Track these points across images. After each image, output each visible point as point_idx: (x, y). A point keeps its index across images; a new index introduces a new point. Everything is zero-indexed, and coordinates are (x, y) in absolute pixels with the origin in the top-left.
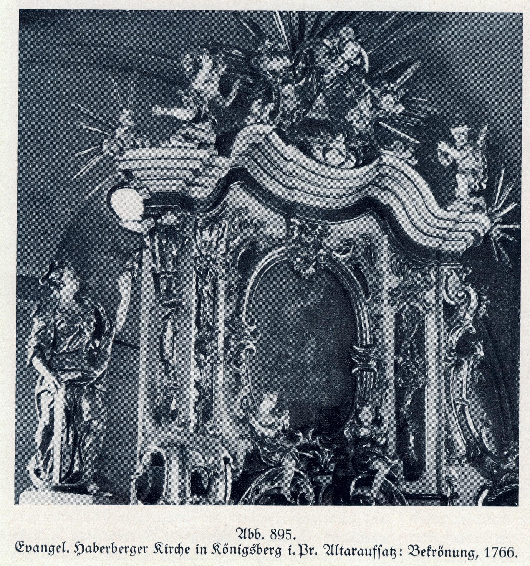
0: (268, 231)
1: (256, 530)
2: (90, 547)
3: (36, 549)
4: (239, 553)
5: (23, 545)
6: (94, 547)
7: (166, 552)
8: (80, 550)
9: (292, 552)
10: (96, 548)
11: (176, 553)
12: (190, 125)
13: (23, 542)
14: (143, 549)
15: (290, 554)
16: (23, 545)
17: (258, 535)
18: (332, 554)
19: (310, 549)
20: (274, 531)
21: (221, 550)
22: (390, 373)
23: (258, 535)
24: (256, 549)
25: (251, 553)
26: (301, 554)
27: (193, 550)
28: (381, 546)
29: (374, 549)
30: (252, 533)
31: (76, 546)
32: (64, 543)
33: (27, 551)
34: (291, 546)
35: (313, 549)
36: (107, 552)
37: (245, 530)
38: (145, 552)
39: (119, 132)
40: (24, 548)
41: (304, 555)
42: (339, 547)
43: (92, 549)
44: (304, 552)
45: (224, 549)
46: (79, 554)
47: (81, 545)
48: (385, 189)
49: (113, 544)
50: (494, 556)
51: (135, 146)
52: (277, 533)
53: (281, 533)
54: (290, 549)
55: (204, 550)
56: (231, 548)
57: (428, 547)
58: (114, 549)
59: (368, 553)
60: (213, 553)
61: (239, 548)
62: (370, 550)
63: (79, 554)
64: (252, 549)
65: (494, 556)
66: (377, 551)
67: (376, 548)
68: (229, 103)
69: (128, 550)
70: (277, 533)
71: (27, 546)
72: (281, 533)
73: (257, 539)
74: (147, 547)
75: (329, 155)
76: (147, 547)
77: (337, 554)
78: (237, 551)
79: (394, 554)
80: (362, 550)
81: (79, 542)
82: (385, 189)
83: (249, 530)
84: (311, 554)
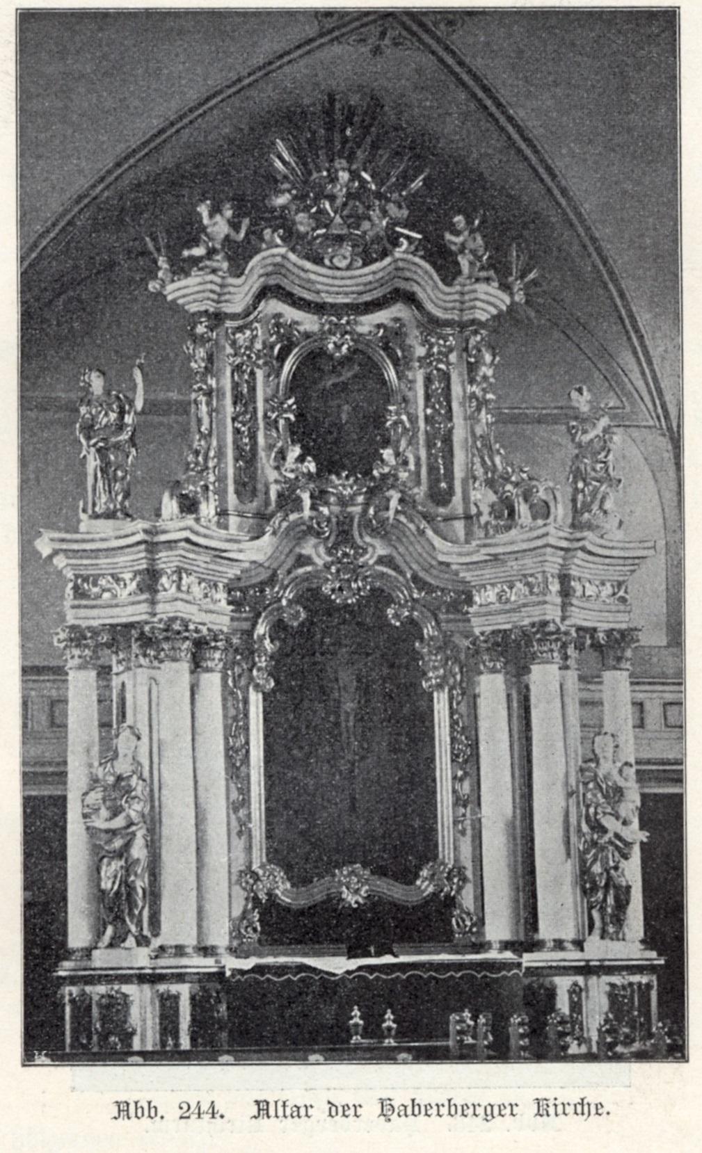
0: (301, 328)
6: (413, 1106)
12: (209, 259)
22: (422, 424)
39: (160, 274)
43: (409, 1111)
51: (173, 281)
58: (453, 1109)
68: (242, 235)
75: (335, 260)
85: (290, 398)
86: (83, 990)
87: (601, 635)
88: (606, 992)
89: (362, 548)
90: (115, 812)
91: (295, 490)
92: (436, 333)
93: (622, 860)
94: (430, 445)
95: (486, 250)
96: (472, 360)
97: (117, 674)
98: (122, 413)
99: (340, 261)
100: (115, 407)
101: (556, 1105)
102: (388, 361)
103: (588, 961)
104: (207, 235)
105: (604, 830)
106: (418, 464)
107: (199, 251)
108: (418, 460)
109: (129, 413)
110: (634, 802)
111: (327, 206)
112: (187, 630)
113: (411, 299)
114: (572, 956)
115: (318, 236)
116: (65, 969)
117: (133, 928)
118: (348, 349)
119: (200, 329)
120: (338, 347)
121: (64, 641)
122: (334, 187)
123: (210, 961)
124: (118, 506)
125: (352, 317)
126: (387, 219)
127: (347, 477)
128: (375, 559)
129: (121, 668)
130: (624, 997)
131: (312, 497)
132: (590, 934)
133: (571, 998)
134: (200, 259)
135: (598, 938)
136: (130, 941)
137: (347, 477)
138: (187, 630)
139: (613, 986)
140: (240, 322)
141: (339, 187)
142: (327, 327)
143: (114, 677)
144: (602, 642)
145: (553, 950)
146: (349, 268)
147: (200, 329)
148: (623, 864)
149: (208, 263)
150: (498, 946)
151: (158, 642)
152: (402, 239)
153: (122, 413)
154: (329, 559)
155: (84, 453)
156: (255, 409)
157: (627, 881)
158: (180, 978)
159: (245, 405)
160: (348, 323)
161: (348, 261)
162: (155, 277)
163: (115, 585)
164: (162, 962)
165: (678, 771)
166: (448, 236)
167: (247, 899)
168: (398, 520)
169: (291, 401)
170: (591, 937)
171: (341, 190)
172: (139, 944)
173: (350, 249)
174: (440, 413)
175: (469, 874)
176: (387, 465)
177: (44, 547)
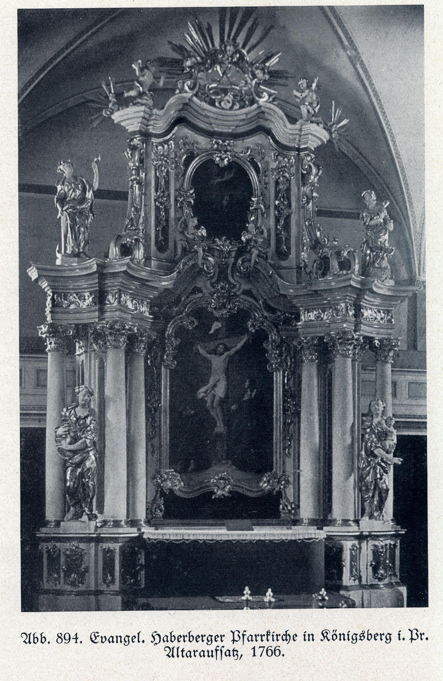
1: (41, 635)
2: (167, 636)
3: (111, 640)
4: (349, 640)
5: (98, 636)
7: (273, 640)
8: (157, 640)
9: (401, 638)
10: (173, 638)
11: (283, 640)
12: (139, 98)
13: (98, 633)
14: (183, 638)
15: (399, 639)
16: (98, 636)
17: (43, 639)
18: (30, 643)
19: (421, 634)
20: (60, 635)
21: (330, 636)
22: (272, 209)
23: (43, 639)
24: (366, 635)
25: (360, 639)
26: (412, 639)
27: (300, 638)
28: (223, 647)
29: (216, 650)
30: (37, 638)
31: (152, 635)
32: (139, 634)
33: (102, 642)
34: (400, 631)
35: (424, 634)
36: (184, 641)
37: (30, 635)
38: (222, 641)
39: (110, 105)
40: (99, 639)
41: (415, 640)
42: (180, 650)
43: (169, 639)
44: (415, 636)
45: (333, 636)
46: (156, 644)
47: (158, 635)
48: (267, 120)
49: (189, 633)
50: (261, 656)
52: (63, 637)
53: (67, 637)
54: (399, 634)
55: (310, 637)
56: (340, 635)
57: (267, 632)
59: (210, 654)
60: (322, 640)
61: (348, 635)
62: (212, 651)
63: (156, 644)
64: (361, 635)
65: (261, 656)
66: (219, 652)
67: (218, 648)
69: (205, 638)
70: (63, 637)
71: (102, 637)
72: (67, 637)
73: (43, 643)
74: (224, 636)
75: (222, 104)
76: (224, 636)
77: (178, 656)
78: (346, 637)
79: (237, 655)
80: (204, 651)
81: (156, 632)
82: (267, 120)
83: (34, 635)
84: (422, 639)
85: (191, 189)
86: (55, 545)
87: (377, 342)
88: (372, 550)
89: (233, 284)
90: (75, 440)
91: (193, 246)
92: (283, 154)
93: (385, 474)
94: (277, 220)
95: (318, 104)
96: (305, 172)
97: (79, 355)
98: (84, 190)
99: (225, 104)
100: (80, 186)
101: (273, 635)
102: (251, 168)
103: (362, 532)
104: (139, 82)
105: (375, 456)
106: (269, 235)
107: (132, 93)
108: (269, 231)
109: (89, 191)
110: (393, 440)
111: (218, 68)
112: (124, 329)
113: (268, 132)
114: (353, 529)
115: (212, 88)
116: (43, 532)
117: (86, 509)
118: (228, 161)
119: (136, 141)
120: (222, 159)
121: (45, 333)
122: (224, 56)
123: (135, 530)
124: (81, 250)
125: (232, 141)
126: (256, 80)
127: (225, 241)
128: (241, 291)
129: (81, 351)
130: (382, 552)
131: (204, 250)
132: (362, 516)
133: (351, 553)
134: (135, 98)
135: (368, 518)
136: (85, 518)
137: (225, 241)
138: (124, 329)
139: (375, 546)
140: (161, 140)
141: (226, 57)
142: (216, 146)
143: (77, 357)
144: (377, 345)
145: (342, 525)
146: (231, 108)
147: (136, 141)
148: (385, 476)
149: (139, 100)
150: (307, 521)
151: (105, 336)
152: (265, 93)
153: (84, 190)
154: (213, 290)
155: (59, 215)
156: (169, 195)
157: (387, 486)
158: (115, 540)
159: (163, 192)
160: (229, 144)
161: (230, 105)
162: (107, 108)
163: (78, 300)
164: (104, 530)
165: (423, 422)
166: (295, 93)
167: (157, 491)
168: (256, 268)
169: (191, 192)
170: (364, 518)
171: (228, 59)
172: (90, 519)
173: (232, 97)
174: (284, 204)
175: (291, 479)
176: (250, 233)
177: (33, 274)
